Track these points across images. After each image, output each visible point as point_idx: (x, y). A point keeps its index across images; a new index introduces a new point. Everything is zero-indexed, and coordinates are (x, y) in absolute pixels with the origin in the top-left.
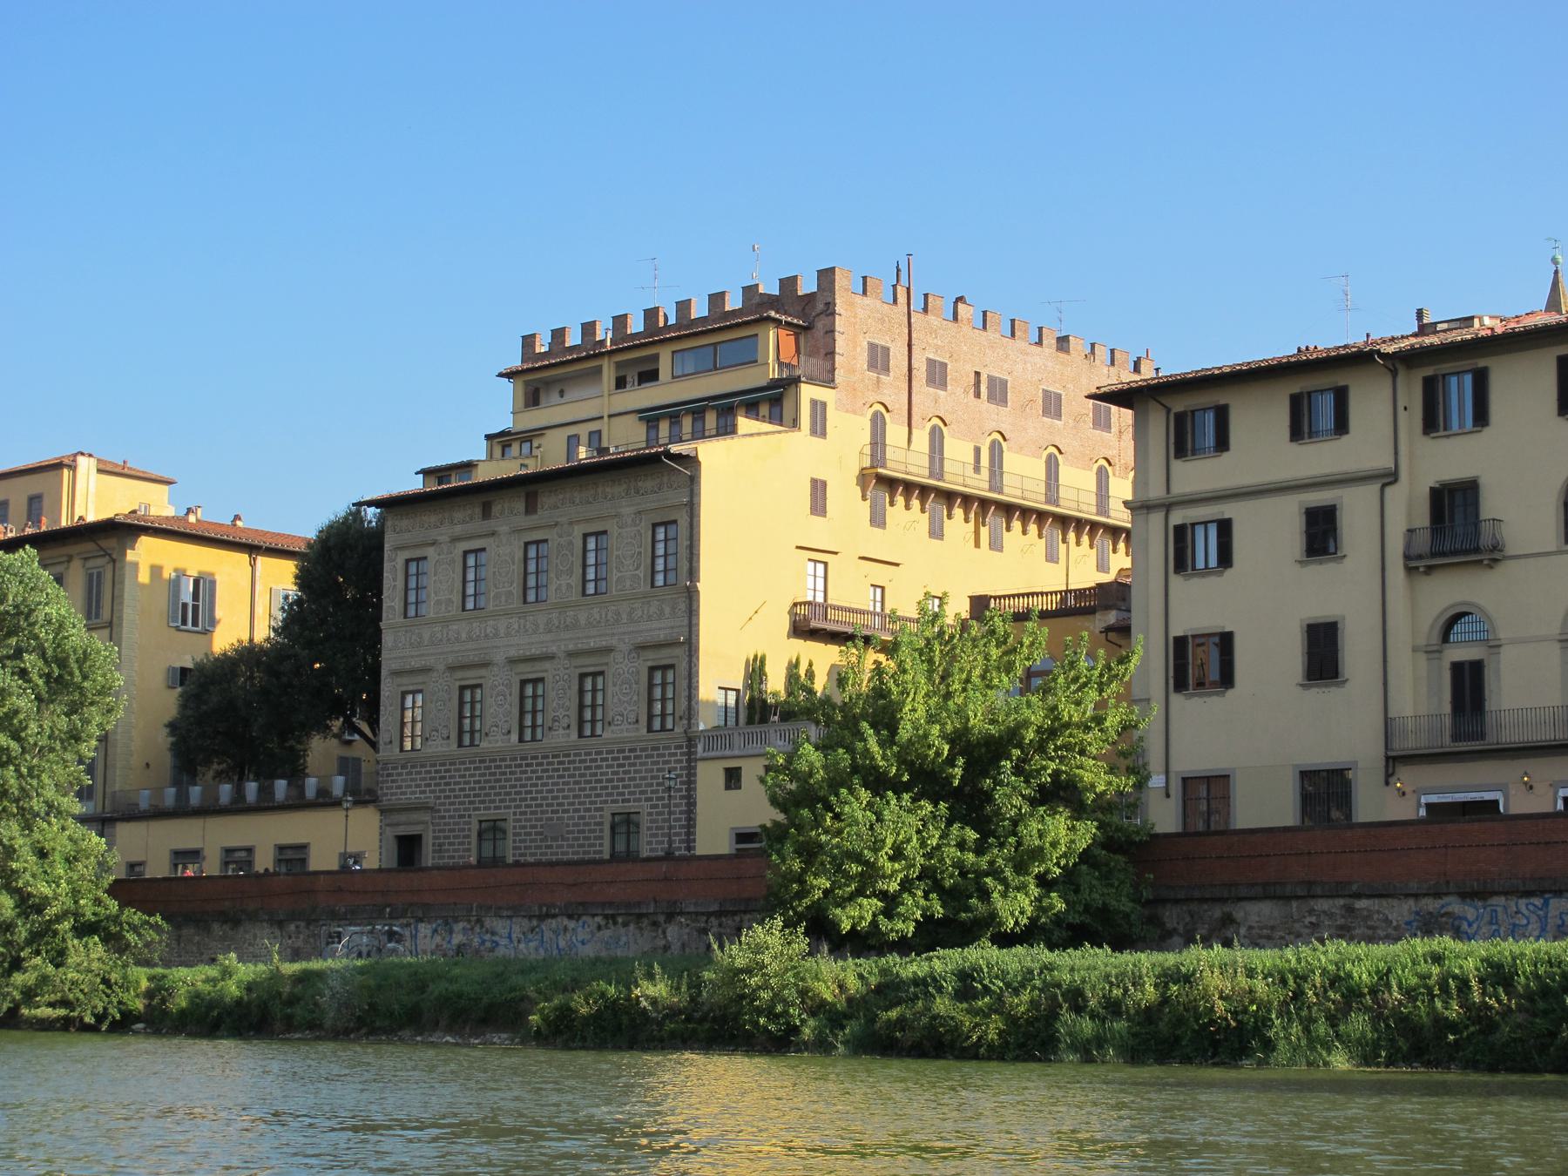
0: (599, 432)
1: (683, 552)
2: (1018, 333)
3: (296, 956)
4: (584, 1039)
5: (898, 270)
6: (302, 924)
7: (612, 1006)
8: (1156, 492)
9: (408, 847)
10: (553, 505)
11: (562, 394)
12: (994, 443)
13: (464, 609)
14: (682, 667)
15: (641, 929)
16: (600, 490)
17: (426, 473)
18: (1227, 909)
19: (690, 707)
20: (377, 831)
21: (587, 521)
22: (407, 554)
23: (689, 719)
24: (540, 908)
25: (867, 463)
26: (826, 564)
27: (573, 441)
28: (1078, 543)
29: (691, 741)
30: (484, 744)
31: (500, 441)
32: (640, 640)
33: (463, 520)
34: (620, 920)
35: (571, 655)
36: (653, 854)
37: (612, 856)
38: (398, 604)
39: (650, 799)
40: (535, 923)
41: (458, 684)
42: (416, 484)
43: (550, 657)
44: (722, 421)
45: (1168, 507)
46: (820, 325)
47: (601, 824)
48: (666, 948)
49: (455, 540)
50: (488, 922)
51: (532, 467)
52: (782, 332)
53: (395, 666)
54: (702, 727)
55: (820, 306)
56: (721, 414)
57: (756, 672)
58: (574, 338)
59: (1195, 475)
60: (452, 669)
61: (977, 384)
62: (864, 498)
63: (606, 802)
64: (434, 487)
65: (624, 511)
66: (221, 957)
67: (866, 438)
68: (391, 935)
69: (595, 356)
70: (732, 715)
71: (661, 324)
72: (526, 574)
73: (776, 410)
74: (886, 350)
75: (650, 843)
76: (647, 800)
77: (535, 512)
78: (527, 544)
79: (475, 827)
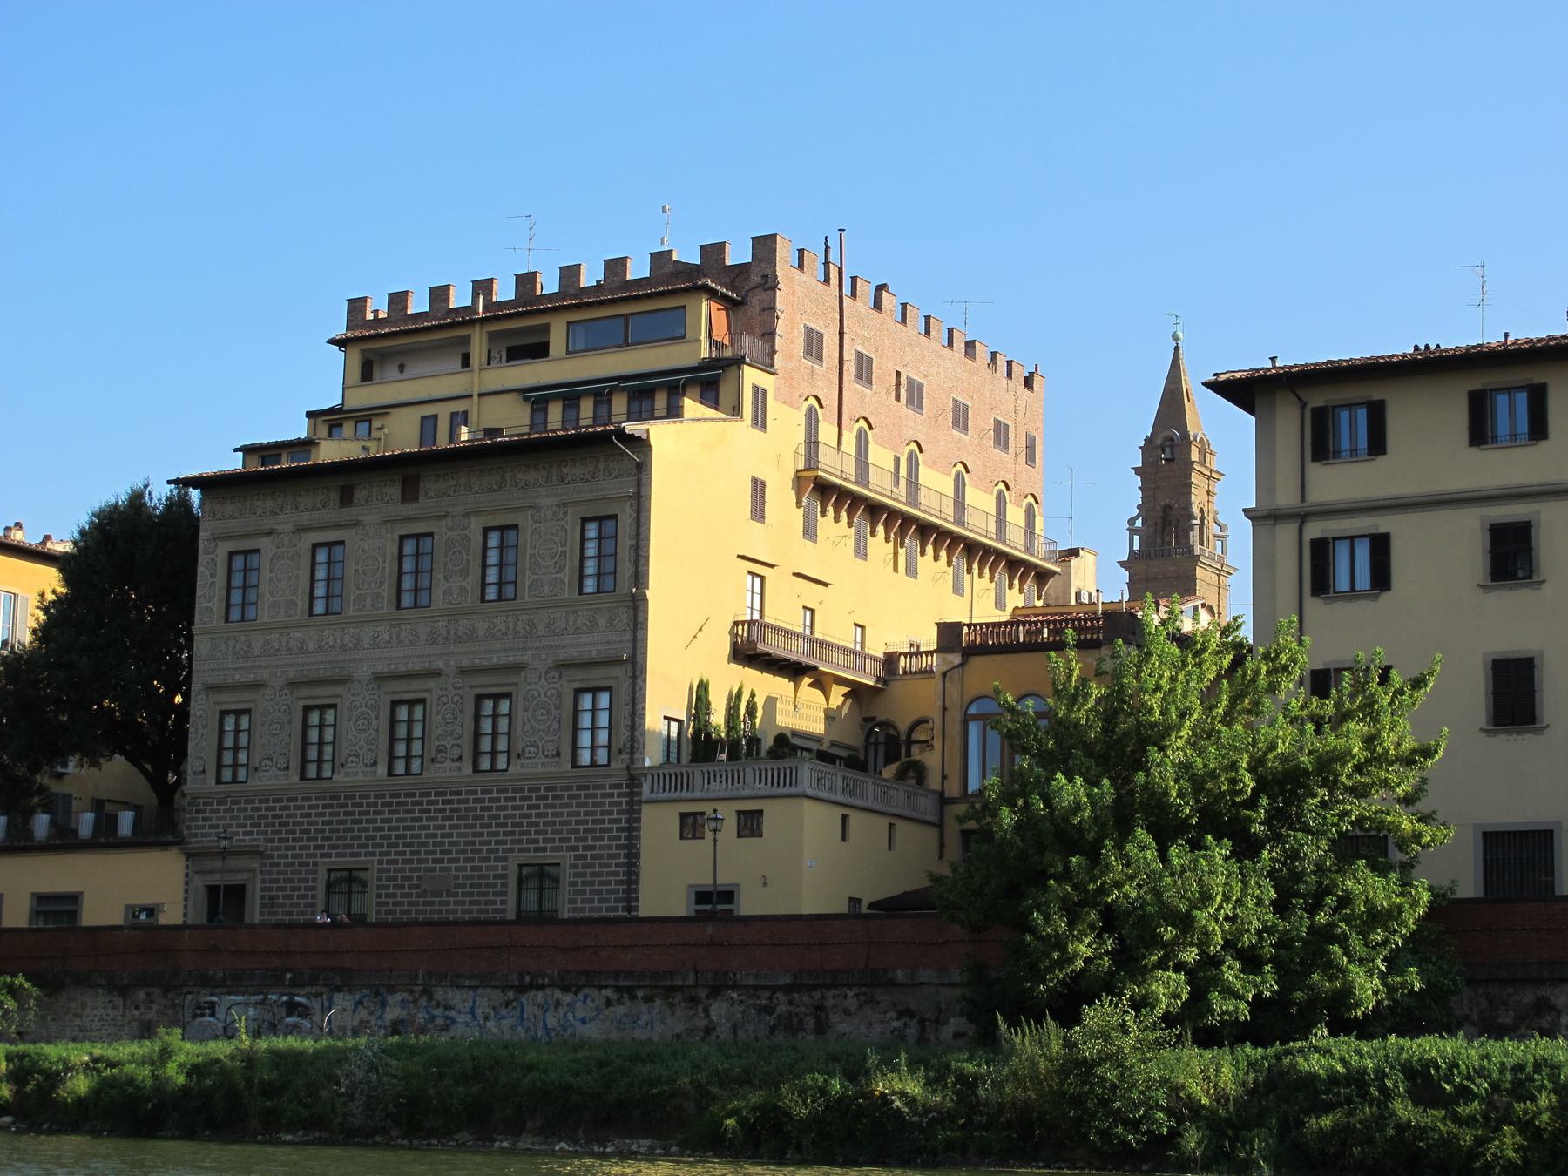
0: (435, 417)
1: (625, 554)
2: (933, 333)
4: (799, 1148)
5: (827, 247)
6: (157, 991)
7: (840, 1105)
8: (1286, 498)
9: (225, 901)
10: (435, 492)
11: (402, 368)
12: (911, 453)
13: (311, 614)
14: (624, 688)
15: (672, 1005)
16: (508, 476)
17: (247, 450)
18: (1541, 993)
19: (632, 739)
20: (182, 879)
22: (232, 546)
23: (632, 753)
24: (521, 976)
25: (801, 466)
26: (762, 578)
28: (981, 575)
29: (634, 778)
31: (328, 420)
33: (315, 508)
34: (640, 994)
35: (463, 672)
36: (578, 915)
37: (519, 913)
38: (218, 607)
39: (575, 848)
40: (511, 995)
41: (301, 703)
42: (235, 463)
43: (437, 674)
44: (636, 406)
45: (1302, 517)
46: (756, 301)
47: (313, 889)
48: (708, 1031)
49: (301, 530)
50: (439, 994)
51: (376, 451)
52: (715, 306)
53: (211, 679)
54: (647, 763)
55: (756, 279)
56: (659, 393)
57: (700, 696)
58: (419, 304)
59: (1337, 482)
60: (293, 685)
61: (898, 384)
62: (799, 504)
63: (512, 850)
64: (256, 467)
65: (546, 508)
66: (162, 1030)
67: (800, 435)
68: (292, 1008)
69: (463, 323)
70: (674, 749)
71: (370, 316)
72: (400, 573)
73: (711, 394)
74: (820, 336)
75: (571, 901)
76: (571, 849)
77: (416, 499)
78: (402, 538)
79: (322, 877)
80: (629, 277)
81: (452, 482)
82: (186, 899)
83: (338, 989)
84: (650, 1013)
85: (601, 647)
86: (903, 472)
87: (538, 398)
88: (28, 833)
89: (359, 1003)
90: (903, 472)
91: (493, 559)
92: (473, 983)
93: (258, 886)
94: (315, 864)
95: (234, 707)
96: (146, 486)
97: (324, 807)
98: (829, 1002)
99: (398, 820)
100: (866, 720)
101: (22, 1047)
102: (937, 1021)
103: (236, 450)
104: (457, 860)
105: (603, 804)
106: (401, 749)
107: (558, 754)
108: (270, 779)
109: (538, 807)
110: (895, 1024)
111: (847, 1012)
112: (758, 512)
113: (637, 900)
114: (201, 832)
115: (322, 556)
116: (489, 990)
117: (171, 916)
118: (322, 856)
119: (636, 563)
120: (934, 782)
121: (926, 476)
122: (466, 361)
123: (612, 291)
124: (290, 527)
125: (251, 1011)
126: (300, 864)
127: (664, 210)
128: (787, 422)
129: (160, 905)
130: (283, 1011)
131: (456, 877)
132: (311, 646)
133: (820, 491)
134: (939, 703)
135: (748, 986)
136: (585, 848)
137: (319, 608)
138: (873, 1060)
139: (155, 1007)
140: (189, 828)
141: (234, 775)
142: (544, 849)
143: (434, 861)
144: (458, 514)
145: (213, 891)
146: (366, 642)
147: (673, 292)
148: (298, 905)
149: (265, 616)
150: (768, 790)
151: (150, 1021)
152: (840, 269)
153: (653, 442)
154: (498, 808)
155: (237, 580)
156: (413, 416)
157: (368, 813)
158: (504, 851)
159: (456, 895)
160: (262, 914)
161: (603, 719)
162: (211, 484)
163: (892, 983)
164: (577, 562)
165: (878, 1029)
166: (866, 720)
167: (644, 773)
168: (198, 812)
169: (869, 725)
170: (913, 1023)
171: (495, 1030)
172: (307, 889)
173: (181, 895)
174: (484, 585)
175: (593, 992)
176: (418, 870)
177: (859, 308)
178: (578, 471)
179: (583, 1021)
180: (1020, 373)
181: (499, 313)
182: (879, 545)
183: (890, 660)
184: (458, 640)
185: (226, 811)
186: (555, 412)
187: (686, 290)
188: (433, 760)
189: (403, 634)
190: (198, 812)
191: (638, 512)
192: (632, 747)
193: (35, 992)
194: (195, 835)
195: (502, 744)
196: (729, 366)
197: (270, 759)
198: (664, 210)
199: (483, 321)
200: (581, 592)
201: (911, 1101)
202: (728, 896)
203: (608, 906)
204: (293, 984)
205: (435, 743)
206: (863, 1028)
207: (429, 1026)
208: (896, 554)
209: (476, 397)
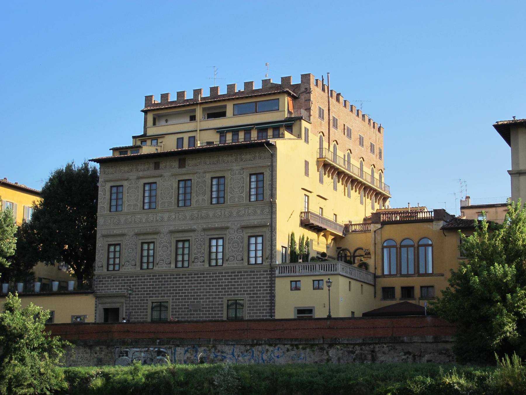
0: (182, 138)
3: (100, 363)
6: (104, 347)
9: (111, 314)
10: (191, 163)
12: (348, 153)
13: (143, 209)
14: (268, 236)
15: (313, 351)
17: (115, 150)
20: (94, 306)
21: (214, 172)
22: (112, 184)
23: (271, 259)
24: (253, 341)
27: (180, 141)
29: (272, 268)
31: (143, 138)
32: (136, 231)
33: (145, 171)
34: (301, 347)
35: (204, 230)
36: (251, 318)
37: (227, 319)
38: (106, 206)
41: (140, 241)
43: (194, 231)
44: (260, 134)
46: (303, 97)
47: (222, 304)
48: (328, 360)
49: (139, 178)
50: (219, 347)
52: (290, 99)
53: (105, 232)
54: (277, 263)
55: (303, 89)
60: (137, 234)
61: (344, 129)
63: (225, 295)
64: (117, 155)
68: (159, 353)
70: (284, 256)
71: (153, 103)
72: (179, 194)
74: (323, 110)
75: (248, 313)
77: (185, 167)
78: (179, 181)
79: (150, 305)
80: (254, 89)
81: (199, 161)
82: (96, 313)
83: (178, 346)
84: (305, 354)
85: (259, 221)
86: (346, 159)
87: (222, 132)
88: (66, 288)
89: (187, 351)
90: (346, 159)
91: (214, 188)
93: (124, 308)
94: (147, 300)
95: (113, 243)
96: (73, 163)
97: (150, 279)
98: (377, 349)
99: (180, 284)
100: (338, 248)
102: (420, 356)
103: (110, 149)
104: (203, 299)
105: (260, 278)
106: (180, 258)
107: (242, 260)
108: (128, 269)
109: (235, 279)
110: (403, 357)
111: (384, 353)
112: (307, 174)
113: (274, 313)
114: (101, 288)
115: (147, 188)
116: (239, 346)
117: (90, 319)
118: (150, 297)
119: (272, 190)
120: (372, 270)
121: (352, 161)
122: (193, 118)
123: (247, 94)
124: (135, 177)
125: (143, 354)
126: (141, 300)
127: (266, 65)
128: (314, 139)
129: (86, 315)
130: (156, 354)
131: (203, 305)
132: (144, 221)
133: (326, 167)
134: (373, 242)
135: (343, 344)
136: (253, 294)
137: (146, 207)
138: (441, 370)
139: (103, 353)
140: (96, 287)
141: (217, 262)
142: (238, 294)
143: (194, 299)
144: (201, 172)
145: (106, 311)
146: (166, 219)
147: (274, 94)
148: (140, 315)
149: (125, 210)
150: (325, 273)
151: (101, 358)
152: (328, 87)
153: (277, 146)
154: (219, 279)
155: (114, 196)
156: (175, 137)
157: (167, 281)
158: (222, 295)
159: (203, 311)
161: (260, 247)
162: (101, 161)
163: (403, 342)
164: (248, 190)
165: (397, 359)
166: (338, 248)
167: (276, 266)
168: (100, 281)
169: (339, 250)
170: (411, 356)
171: (242, 361)
172: (144, 309)
173: (94, 312)
174: (212, 198)
175: (282, 346)
176: (188, 302)
177: (333, 101)
178: (248, 157)
179: (278, 357)
180: (377, 126)
181: (205, 101)
182: (340, 186)
183: (346, 228)
184: (202, 218)
185: (111, 281)
186: (229, 137)
187: (279, 93)
188: (193, 262)
189: (180, 216)
190: (100, 281)
191: (272, 171)
192: (271, 257)
193: (73, 346)
194: (99, 290)
195: (186, 258)
196: (297, 120)
197: (163, 261)
198: (266, 65)
199: (201, 104)
200: (250, 201)
201: (461, 386)
202: (310, 311)
203: (264, 315)
204: (160, 344)
205: (194, 256)
206: (390, 359)
207: (215, 359)
208: (345, 189)
209: (198, 131)
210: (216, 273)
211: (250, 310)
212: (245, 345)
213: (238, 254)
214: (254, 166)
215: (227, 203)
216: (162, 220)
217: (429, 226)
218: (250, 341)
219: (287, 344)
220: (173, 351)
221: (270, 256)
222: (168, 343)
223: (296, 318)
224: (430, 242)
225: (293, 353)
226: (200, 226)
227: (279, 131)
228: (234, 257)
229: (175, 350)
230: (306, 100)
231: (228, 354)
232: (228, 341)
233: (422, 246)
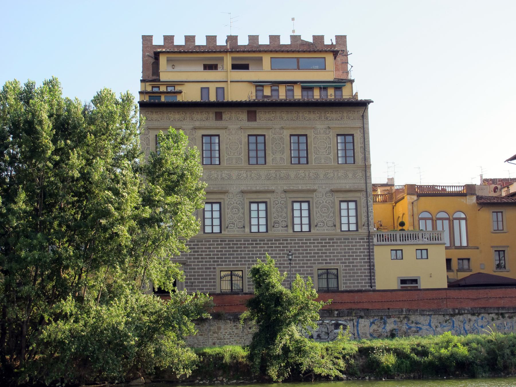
10: (264, 118)
14: (362, 202)
24: (454, 310)
27: (205, 91)
30: (226, 233)
34: (507, 315)
36: (348, 289)
50: (413, 318)
63: (315, 263)
75: (344, 283)
81: (273, 115)
83: (362, 317)
92: (430, 313)
94: (214, 268)
101: (470, 336)
116: (437, 316)
118: (218, 265)
146: (234, 177)
158: (310, 263)
160: (249, 288)
175: (486, 316)
184: (281, 178)
186: (267, 91)
192: (368, 224)
197: (234, 224)
198: (293, 19)
204: (339, 315)
207: (409, 331)
210: (302, 240)
211: (346, 280)
212: (444, 315)
213: (327, 219)
214: (343, 126)
215: (312, 163)
216: (230, 178)
217: (462, 200)
218: (450, 310)
219: (491, 313)
220: (356, 324)
221: (366, 223)
222: (349, 314)
223: (400, 288)
224: (463, 216)
225: (499, 322)
226: (279, 188)
227: (313, 92)
228: (324, 222)
229: (358, 323)
230: (343, 63)
231: (423, 325)
232: (423, 311)
233: (456, 219)
